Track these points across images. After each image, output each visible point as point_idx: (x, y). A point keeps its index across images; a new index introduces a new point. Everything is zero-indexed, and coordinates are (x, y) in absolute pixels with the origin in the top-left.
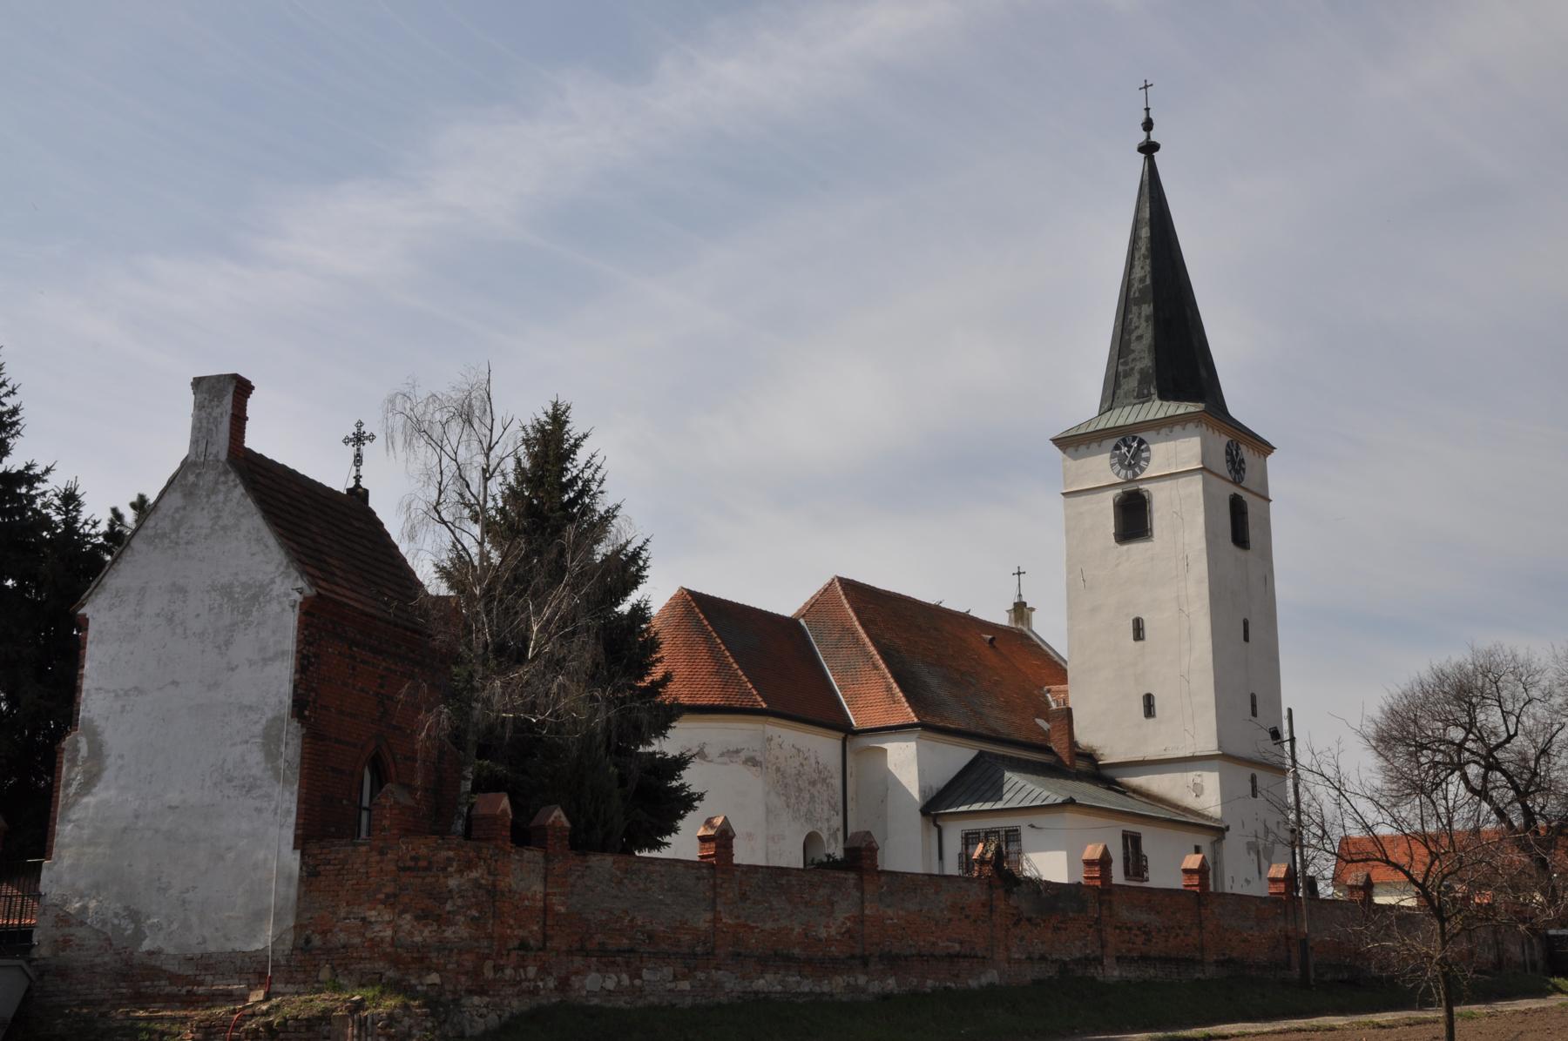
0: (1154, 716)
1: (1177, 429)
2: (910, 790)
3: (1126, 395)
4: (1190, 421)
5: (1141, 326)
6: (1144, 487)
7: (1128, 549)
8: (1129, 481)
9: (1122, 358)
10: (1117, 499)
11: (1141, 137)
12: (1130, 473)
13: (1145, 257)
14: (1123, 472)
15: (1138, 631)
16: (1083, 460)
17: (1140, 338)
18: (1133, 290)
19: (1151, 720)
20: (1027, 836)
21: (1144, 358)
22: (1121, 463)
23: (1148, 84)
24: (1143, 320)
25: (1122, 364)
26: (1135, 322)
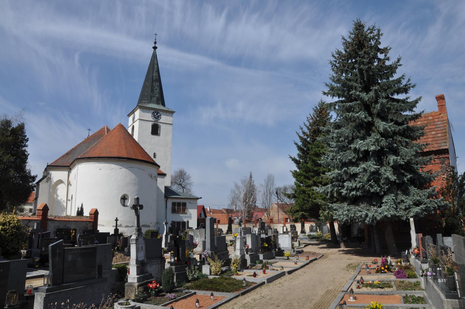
1: (168, 114)
3: (154, 101)
8: (156, 121)
11: (154, 45)
12: (156, 120)
14: (154, 119)
17: (156, 89)
20: (188, 205)
24: (157, 86)
26: (155, 86)
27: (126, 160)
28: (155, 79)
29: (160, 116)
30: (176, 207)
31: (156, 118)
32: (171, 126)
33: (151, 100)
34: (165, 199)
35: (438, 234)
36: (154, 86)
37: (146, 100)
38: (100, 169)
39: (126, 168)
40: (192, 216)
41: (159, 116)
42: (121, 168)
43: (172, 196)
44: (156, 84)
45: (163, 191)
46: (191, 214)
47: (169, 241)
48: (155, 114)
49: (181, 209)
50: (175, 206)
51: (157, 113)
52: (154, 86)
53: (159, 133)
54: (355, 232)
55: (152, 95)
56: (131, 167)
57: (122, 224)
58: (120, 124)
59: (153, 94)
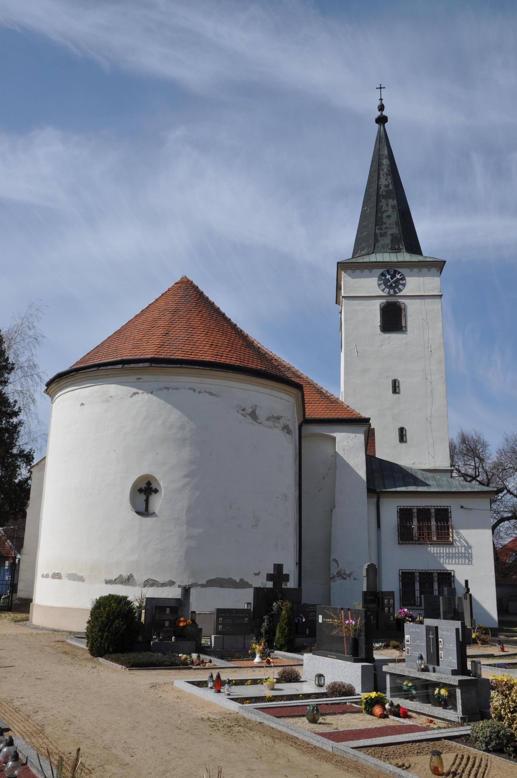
0: (406, 442)
1: (425, 270)
2: (357, 471)
3: (383, 246)
4: (434, 266)
5: (389, 211)
6: (401, 300)
7: (389, 337)
8: (390, 296)
9: (377, 226)
10: (382, 305)
11: (378, 114)
12: (392, 291)
13: (387, 175)
14: (387, 290)
15: (395, 387)
16: (358, 279)
17: (389, 217)
18: (381, 191)
19: (403, 445)
21: (393, 228)
22: (385, 284)
23: (382, 86)
24: (390, 207)
25: (378, 229)
26: (384, 208)
27: (147, 364)
28: (386, 191)
29: (403, 279)
30: (415, 524)
31: (391, 287)
32: (438, 300)
33: (375, 245)
34: (368, 497)
35: (272, 582)
36: (383, 210)
37: (364, 250)
38: (82, 404)
39: (152, 393)
40: (474, 551)
41: (398, 280)
42: (135, 394)
43: (396, 487)
44: (387, 205)
45: (362, 472)
46: (471, 543)
47: (461, 640)
48: (388, 277)
49: (434, 528)
50: (411, 520)
51: (392, 273)
52: (383, 210)
53: (403, 324)
54: (44, 575)
55: (378, 231)
56: (168, 388)
57: (135, 576)
58: (182, 278)
59: (381, 229)
